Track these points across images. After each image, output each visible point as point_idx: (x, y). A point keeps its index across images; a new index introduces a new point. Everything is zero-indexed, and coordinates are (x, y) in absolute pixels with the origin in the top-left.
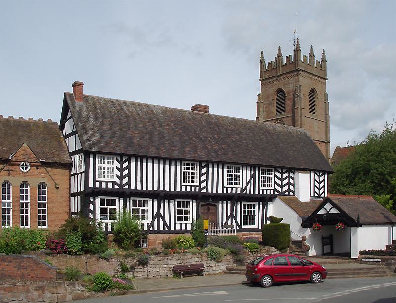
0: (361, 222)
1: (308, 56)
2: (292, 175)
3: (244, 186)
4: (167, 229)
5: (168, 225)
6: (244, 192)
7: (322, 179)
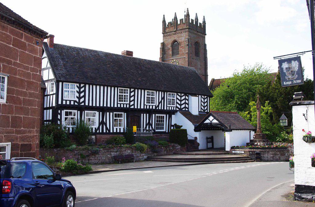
2: (187, 98)
4: (108, 132)
6: (157, 109)
7: (206, 100)
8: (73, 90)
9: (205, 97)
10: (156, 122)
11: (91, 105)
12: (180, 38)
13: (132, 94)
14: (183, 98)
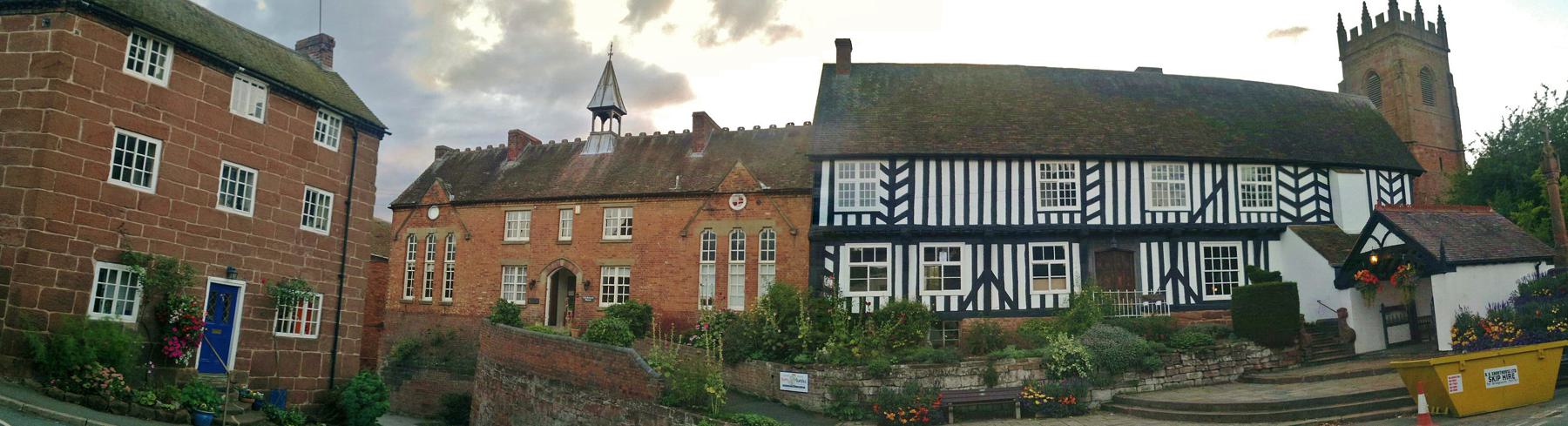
0: (1450, 258)
1: (1413, 13)
2: (1322, 179)
4: (1193, 301)
5: (1012, 298)
6: (1199, 221)
7: (1397, 185)
8: (870, 180)
9: (1394, 175)
10: (1203, 270)
11: (932, 221)
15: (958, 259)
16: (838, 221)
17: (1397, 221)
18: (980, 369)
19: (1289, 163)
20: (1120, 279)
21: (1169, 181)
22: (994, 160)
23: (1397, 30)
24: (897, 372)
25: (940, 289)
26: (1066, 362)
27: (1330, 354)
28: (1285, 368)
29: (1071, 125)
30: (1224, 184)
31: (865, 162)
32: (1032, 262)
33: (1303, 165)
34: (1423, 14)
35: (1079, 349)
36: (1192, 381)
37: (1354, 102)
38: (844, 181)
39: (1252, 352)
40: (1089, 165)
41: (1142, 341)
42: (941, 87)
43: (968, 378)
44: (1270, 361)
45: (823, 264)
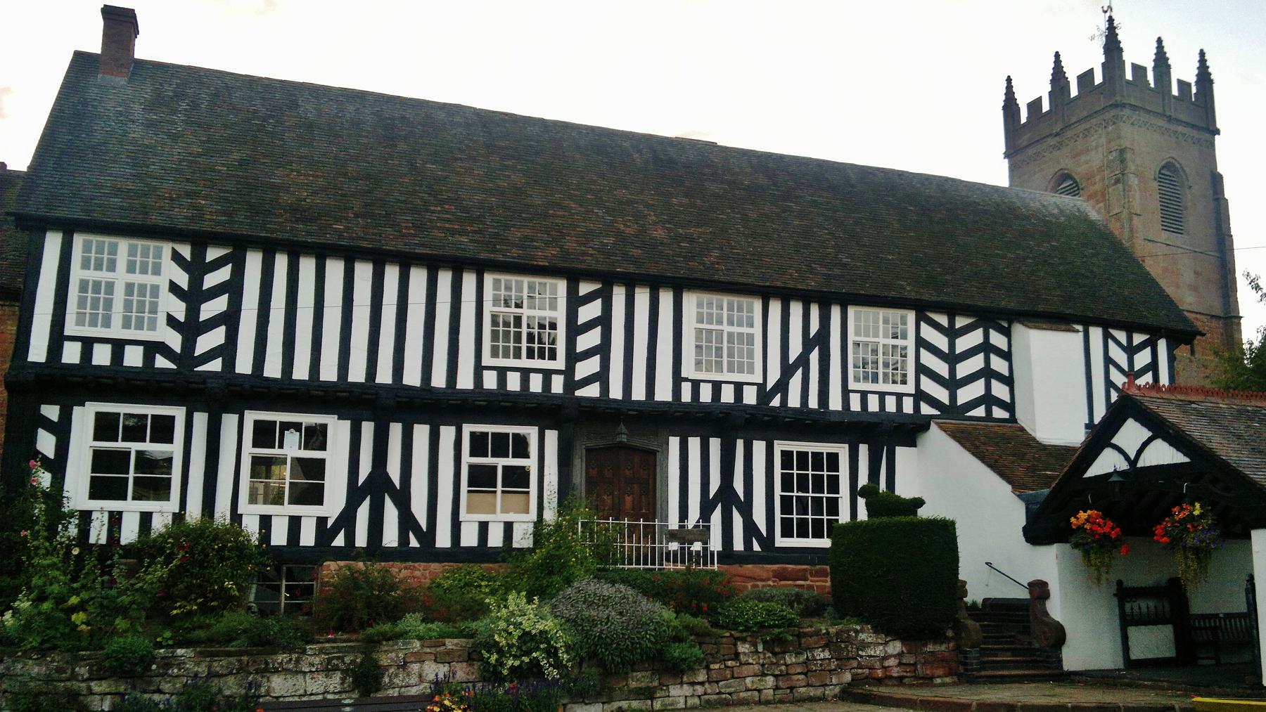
1: (1149, 65)
2: (997, 339)
3: (774, 376)
4: (756, 547)
6: (776, 402)
7: (1143, 358)
8: (149, 279)
9: (1138, 338)
10: (778, 492)
11: (273, 369)
12: (1083, 158)
13: (590, 311)
14: (963, 344)
15: (323, 447)
16: (72, 353)
17: (1172, 415)
18: (347, 660)
19: (939, 308)
20: (628, 499)
21: (726, 328)
22: (406, 262)
23: (1118, 98)
24: (167, 663)
25: (282, 504)
26: (519, 648)
27: (1017, 665)
28: (927, 681)
29: (554, 216)
30: (822, 339)
31: (140, 243)
32: (467, 459)
33: (965, 312)
34: (1169, 67)
35: (548, 624)
36: (756, 693)
37: (1058, 207)
38: (92, 275)
39: (868, 645)
40: (585, 288)
41: (668, 614)
42: (310, 126)
43: (321, 678)
44: (900, 664)
45: (33, 439)
